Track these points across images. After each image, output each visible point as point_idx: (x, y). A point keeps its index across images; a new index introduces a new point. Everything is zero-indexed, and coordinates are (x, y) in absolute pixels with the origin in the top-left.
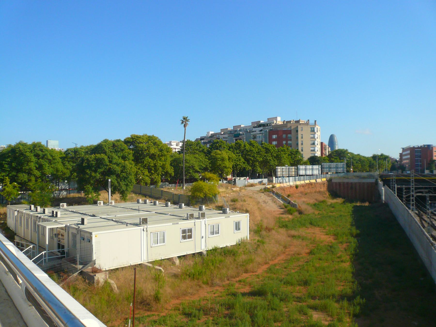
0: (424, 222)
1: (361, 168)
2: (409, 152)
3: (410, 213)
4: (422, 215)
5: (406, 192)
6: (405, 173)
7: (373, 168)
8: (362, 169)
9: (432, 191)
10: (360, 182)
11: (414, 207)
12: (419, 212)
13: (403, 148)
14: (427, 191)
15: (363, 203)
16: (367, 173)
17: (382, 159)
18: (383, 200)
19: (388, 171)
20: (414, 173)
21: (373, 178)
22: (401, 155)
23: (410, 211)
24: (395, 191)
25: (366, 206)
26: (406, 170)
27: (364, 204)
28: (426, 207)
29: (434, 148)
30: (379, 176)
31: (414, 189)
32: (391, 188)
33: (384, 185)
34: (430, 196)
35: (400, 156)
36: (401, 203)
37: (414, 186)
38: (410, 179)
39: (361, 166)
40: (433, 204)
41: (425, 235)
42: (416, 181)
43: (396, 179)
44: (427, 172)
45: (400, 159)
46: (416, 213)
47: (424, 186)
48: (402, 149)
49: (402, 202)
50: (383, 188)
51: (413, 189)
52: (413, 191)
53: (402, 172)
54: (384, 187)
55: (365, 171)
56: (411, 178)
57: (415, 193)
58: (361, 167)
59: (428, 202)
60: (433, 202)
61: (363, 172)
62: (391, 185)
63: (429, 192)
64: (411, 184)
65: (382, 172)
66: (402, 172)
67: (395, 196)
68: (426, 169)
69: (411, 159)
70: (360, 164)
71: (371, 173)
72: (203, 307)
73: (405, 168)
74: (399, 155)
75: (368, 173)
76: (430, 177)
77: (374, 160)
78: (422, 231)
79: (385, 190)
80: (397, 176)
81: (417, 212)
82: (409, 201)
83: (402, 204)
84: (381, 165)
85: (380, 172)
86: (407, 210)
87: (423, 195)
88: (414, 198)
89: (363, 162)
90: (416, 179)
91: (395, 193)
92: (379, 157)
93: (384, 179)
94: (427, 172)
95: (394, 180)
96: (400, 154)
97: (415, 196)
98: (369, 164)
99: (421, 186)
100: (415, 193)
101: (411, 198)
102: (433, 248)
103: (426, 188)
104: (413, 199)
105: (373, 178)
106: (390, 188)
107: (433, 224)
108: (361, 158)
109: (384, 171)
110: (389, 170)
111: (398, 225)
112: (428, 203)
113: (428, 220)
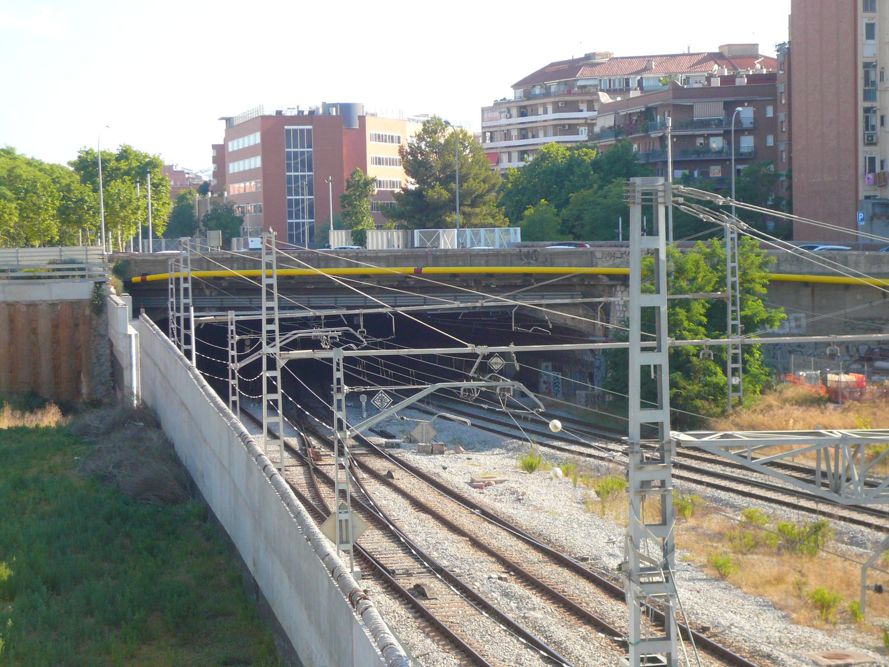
0: (323, 489)
1: (18, 226)
2: (255, 139)
3: (259, 449)
4: (318, 457)
5: (241, 345)
6: (237, 249)
7: (79, 222)
8: (22, 227)
9: (358, 335)
10: (10, 299)
11: (279, 419)
12: (303, 442)
13: (228, 120)
14: (335, 334)
15: (32, 411)
16: (47, 249)
17: (127, 173)
18: (132, 393)
19: (155, 236)
20: (275, 249)
21: (83, 276)
22: (221, 155)
23: (259, 442)
24: (188, 341)
25: (47, 430)
26: (246, 234)
27: (33, 417)
28: (328, 417)
29: (369, 121)
30: (112, 265)
31: (275, 327)
32: (173, 326)
33: (136, 314)
34: (346, 359)
35: (215, 160)
36: (216, 403)
37: (277, 315)
38: (258, 278)
39: (16, 213)
40: (363, 399)
41: (325, 556)
42: (288, 285)
43: (196, 283)
44: (338, 239)
45: (215, 174)
46: (288, 447)
47: (322, 313)
48: (224, 121)
49: (219, 399)
50: (131, 330)
51: (270, 327)
52: (271, 340)
53: (227, 245)
54: (136, 322)
55: (37, 243)
56: (263, 272)
57: (282, 349)
58: (17, 219)
59: (339, 390)
60: (369, 388)
61: (28, 244)
62: (171, 313)
63: (346, 340)
64: (265, 304)
65: (128, 243)
66: (227, 245)
67: (190, 368)
68: (338, 227)
69: (267, 173)
70: (14, 205)
71: (68, 252)
72: (804, 556)
73: (240, 220)
74: (211, 153)
75: (53, 253)
76: (350, 265)
77: (84, 181)
78: (308, 539)
79: (141, 337)
80: (199, 263)
81: (294, 442)
82: (256, 389)
83: (221, 410)
84: (123, 207)
85: (116, 244)
86: (241, 434)
87: (319, 355)
88: (277, 373)
89: (27, 191)
90: (290, 277)
91: (188, 354)
92: (113, 164)
93: (136, 279)
94: (338, 239)
95: (183, 285)
96: (215, 147)
97: (281, 363)
98: (57, 203)
99: (311, 313)
100: (282, 349)
101: (266, 374)
102: (358, 617)
103: (333, 321)
104: (275, 378)
105: (83, 276)
106: (164, 325)
107: (366, 497)
108: (18, 171)
109: (136, 239)
110: (160, 231)
111: (207, 514)
112: (337, 397)
113: (341, 477)
